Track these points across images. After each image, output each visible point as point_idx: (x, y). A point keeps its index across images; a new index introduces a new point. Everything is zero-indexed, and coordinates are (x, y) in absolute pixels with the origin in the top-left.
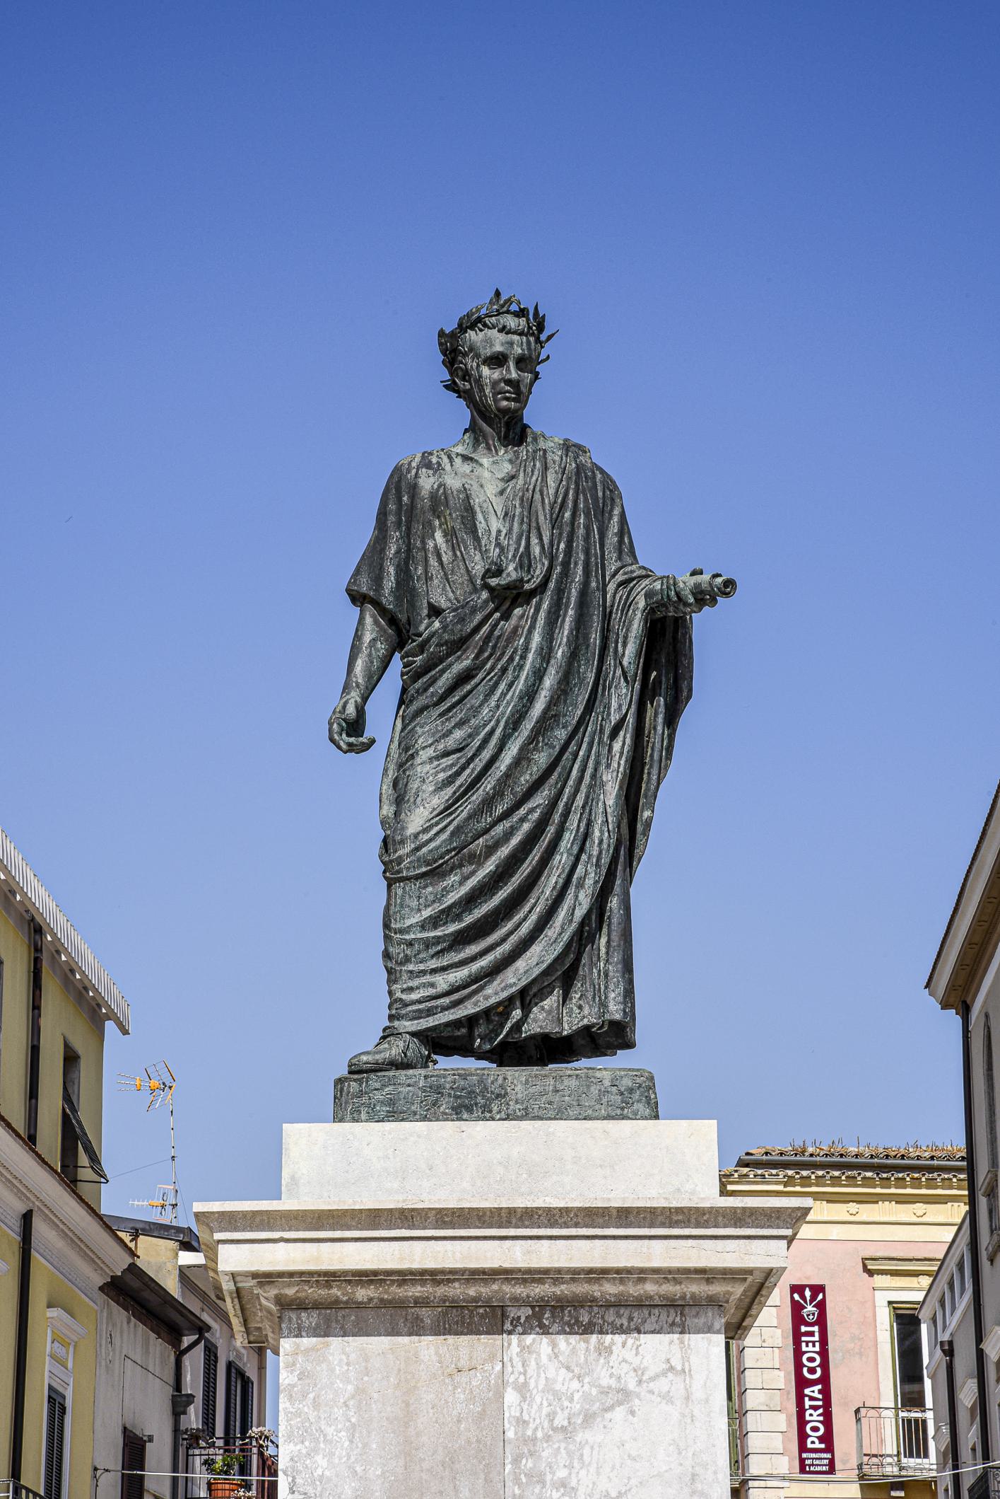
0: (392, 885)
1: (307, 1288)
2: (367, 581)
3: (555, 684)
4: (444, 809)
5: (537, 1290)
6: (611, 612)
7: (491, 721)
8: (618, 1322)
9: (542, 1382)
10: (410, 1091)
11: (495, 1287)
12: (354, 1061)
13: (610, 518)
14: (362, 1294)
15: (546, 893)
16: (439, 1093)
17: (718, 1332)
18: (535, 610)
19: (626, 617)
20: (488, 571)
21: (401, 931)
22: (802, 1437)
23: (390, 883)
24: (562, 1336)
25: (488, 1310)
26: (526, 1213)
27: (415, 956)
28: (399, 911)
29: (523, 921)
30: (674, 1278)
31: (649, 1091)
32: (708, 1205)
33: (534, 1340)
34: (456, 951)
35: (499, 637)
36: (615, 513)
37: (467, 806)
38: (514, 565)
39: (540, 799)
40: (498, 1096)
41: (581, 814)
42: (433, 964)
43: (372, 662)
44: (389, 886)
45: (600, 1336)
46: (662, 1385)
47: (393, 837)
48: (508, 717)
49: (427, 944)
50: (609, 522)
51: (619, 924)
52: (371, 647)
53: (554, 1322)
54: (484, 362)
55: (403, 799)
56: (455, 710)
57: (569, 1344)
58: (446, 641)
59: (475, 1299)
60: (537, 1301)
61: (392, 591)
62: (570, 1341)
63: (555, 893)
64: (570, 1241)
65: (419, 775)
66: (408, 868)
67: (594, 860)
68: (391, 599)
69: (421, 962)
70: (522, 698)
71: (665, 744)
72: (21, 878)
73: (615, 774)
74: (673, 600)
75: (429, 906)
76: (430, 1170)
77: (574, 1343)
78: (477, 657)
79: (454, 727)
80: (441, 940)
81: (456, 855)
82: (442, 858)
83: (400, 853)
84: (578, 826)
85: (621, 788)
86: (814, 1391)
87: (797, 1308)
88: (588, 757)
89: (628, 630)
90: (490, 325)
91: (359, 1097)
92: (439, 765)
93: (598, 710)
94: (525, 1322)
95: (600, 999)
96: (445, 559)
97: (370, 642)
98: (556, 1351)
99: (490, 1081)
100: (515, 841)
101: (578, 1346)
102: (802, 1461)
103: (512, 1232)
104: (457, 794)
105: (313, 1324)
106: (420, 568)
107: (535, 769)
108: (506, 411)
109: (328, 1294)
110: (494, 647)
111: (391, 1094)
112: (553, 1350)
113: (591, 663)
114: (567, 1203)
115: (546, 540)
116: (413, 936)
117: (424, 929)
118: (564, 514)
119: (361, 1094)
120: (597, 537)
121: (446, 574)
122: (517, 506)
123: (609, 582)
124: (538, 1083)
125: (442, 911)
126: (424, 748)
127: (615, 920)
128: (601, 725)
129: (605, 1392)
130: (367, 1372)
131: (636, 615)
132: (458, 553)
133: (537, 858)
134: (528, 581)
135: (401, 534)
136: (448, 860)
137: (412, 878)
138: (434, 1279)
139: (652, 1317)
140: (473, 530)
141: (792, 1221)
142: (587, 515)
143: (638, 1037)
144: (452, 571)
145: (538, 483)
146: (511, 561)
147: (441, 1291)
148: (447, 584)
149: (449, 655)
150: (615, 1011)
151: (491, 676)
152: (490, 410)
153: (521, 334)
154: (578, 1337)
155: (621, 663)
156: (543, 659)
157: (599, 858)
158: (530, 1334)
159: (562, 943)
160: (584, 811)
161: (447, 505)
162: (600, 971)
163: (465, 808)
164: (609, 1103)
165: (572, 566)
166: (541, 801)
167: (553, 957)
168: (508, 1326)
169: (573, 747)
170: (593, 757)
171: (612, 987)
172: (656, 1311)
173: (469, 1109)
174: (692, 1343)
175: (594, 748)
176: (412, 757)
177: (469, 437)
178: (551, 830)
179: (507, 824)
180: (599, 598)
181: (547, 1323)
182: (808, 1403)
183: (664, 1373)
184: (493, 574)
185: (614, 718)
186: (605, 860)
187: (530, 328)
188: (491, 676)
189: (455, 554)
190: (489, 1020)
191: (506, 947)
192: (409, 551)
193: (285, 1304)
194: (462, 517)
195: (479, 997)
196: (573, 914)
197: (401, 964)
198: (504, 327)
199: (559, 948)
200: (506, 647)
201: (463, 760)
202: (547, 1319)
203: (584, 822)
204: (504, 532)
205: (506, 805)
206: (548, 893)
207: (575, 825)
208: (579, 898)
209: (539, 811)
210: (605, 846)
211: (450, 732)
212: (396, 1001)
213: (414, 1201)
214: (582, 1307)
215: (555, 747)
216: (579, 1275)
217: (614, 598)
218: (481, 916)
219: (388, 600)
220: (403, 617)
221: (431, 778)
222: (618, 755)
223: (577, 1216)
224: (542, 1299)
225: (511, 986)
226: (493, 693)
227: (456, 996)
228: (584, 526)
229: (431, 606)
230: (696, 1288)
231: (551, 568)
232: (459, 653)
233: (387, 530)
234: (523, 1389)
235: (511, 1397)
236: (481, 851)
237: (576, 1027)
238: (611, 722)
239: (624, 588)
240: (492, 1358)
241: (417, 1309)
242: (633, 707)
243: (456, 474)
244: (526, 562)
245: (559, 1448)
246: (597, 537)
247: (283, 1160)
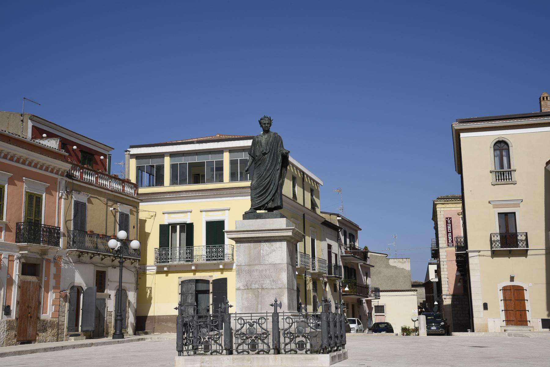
5: (264, 239)
22: (448, 241)
39: (269, 179)
42: (256, 200)
46: (279, 249)
49: (255, 197)
86: (450, 234)
87: (447, 221)
100: (266, 184)
102: (448, 245)
129: (272, 250)
130: (245, 249)
147: (253, 239)
150: (279, 204)
153: (267, 120)
169: (273, 172)
173: (258, 218)
182: (449, 236)
183: (279, 248)
185: (278, 168)
191: (264, 198)
195: (261, 204)
231: (270, 150)
234: (263, 250)
235: (262, 251)
240: (259, 247)
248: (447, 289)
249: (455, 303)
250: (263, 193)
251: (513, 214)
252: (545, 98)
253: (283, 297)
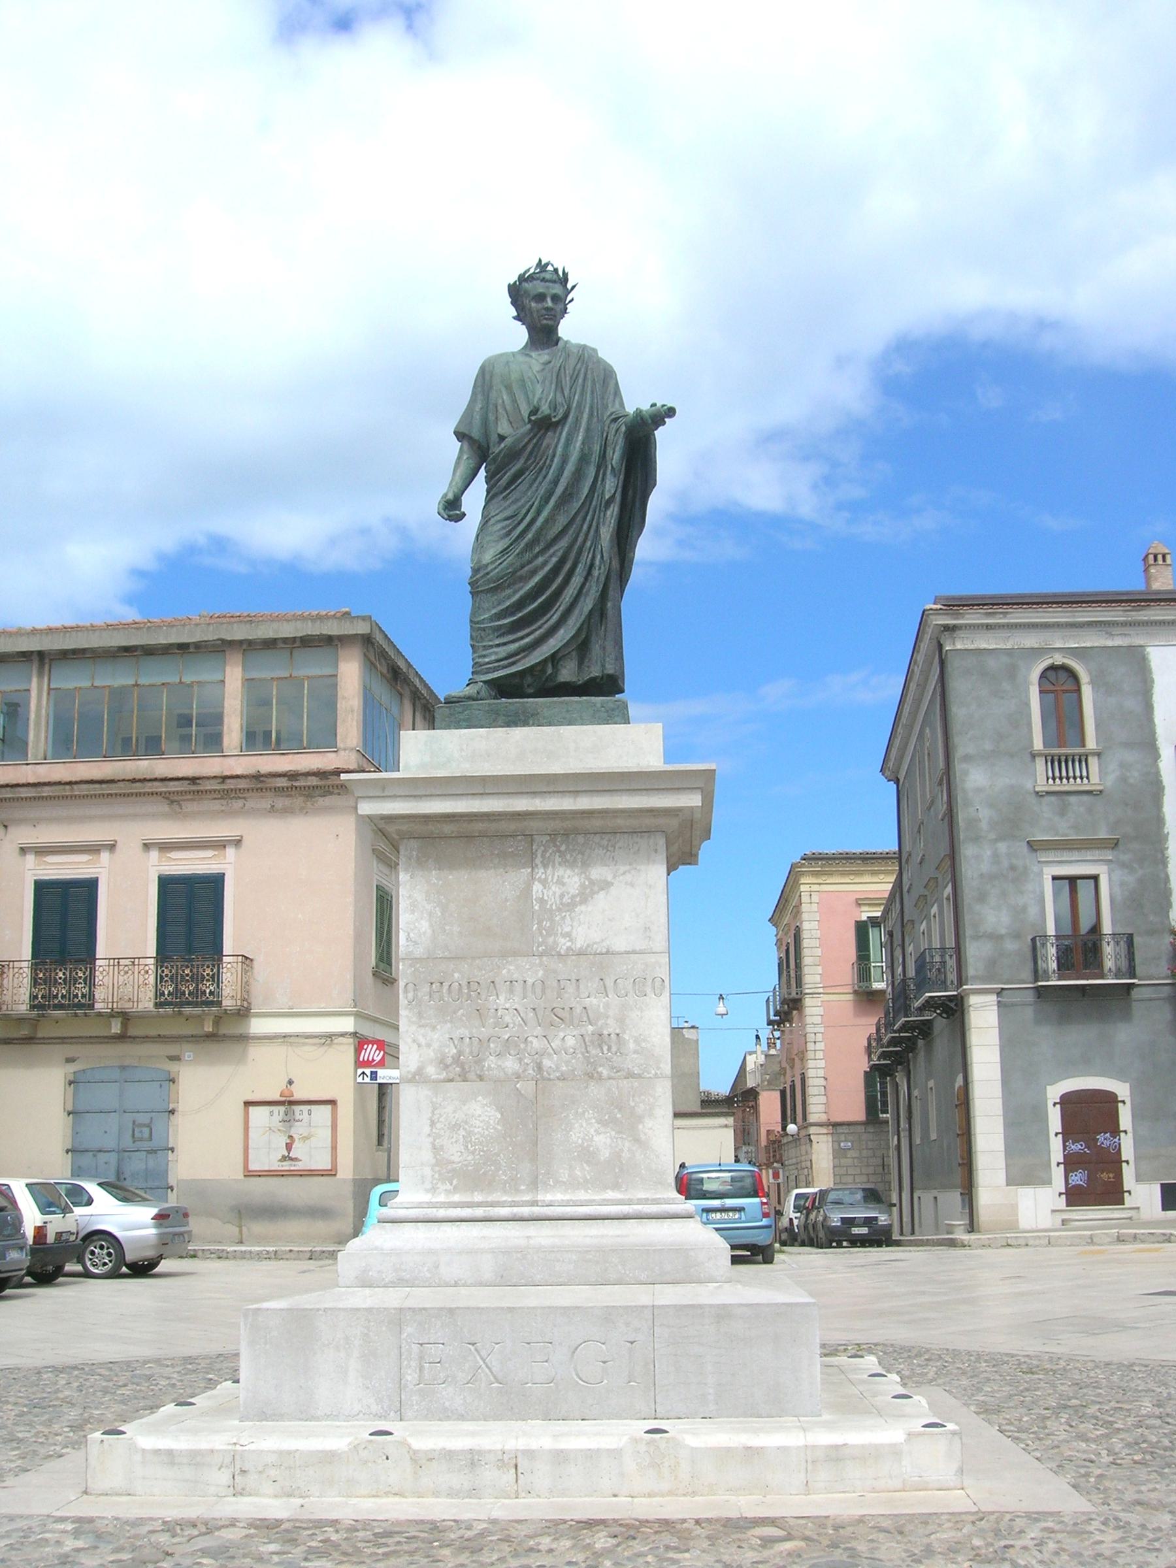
5: (551, 825)
9: (556, 877)
11: (525, 823)
39: (563, 543)
42: (497, 642)
78: (525, 463)
88: (593, 520)
110: (536, 458)
134: (555, 417)
136: (507, 580)
143: (626, 688)
150: (610, 669)
169: (582, 514)
181: (558, 844)
190: (532, 675)
191: (542, 631)
201: (516, 522)
209: (562, 551)
227: (510, 660)
242: (620, 490)
245: (565, 916)
247: (438, 776)
248: (821, 1108)
249: (842, 1144)
250: (535, 611)
251: (1092, 881)
252: (1160, 557)
253: (649, 1123)
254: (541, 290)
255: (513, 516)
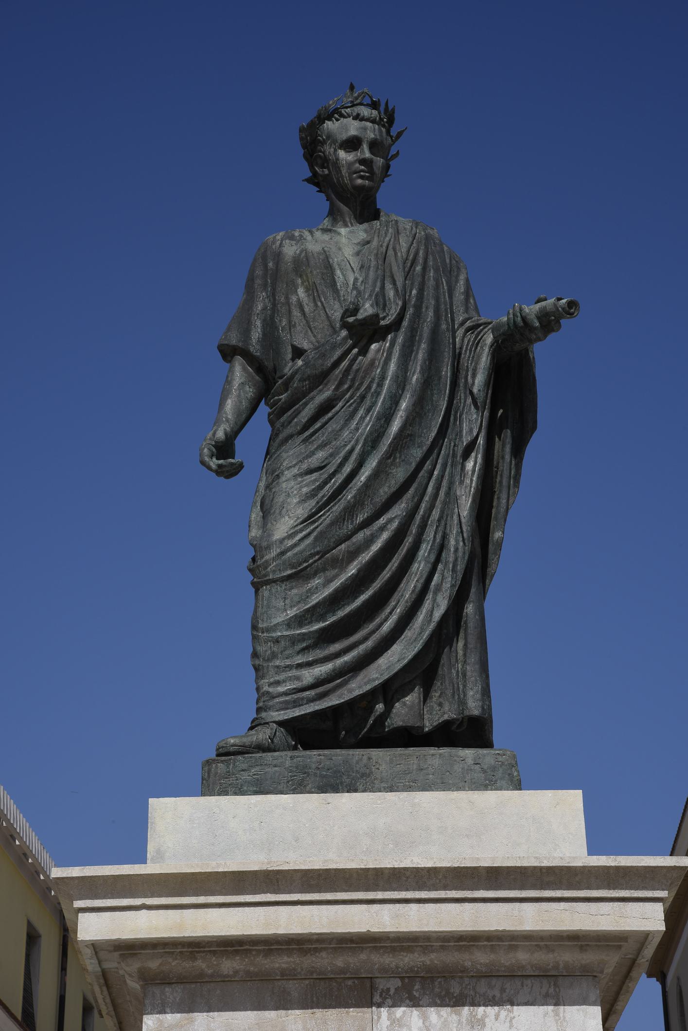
0: (259, 590)
1: (170, 960)
2: (236, 335)
3: (411, 405)
4: (307, 517)
5: (407, 960)
6: (460, 354)
7: (350, 442)
8: (490, 993)
10: (276, 771)
11: (363, 956)
12: (222, 744)
13: (457, 281)
14: (228, 965)
15: (406, 596)
16: (305, 773)
17: (594, 1004)
18: (390, 344)
19: (474, 353)
20: (346, 311)
21: (268, 630)
23: (257, 587)
24: (432, 1009)
25: (356, 982)
26: (439, 590)
27: (282, 652)
28: (266, 612)
29: (385, 622)
30: (546, 945)
31: (512, 769)
32: (580, 864)
33: (404, 1012)
34: (320, 648)
35: (358, 371)
36: (460, 278)
37: (329, 515)
38: (371, 302)
39: (399, 510)
40: (363, 775)
41: (437, 527)
42: (300, 659)
43: (241, 402)
44: (257, 591)
45: (472, 1008)
47: (260, 544)
48: (367, 436)
50: (456, 285)
51: (475, 628)
52: (240, 390)
53: (424, 994)
54: (341, 147)
55: (269, 512)
56: (317, 434)
57: (440, 1016)
58: (309, 376)
59: (342, 971)
60: (406, 972)
61: (258, 341)
62: (442, 1013)
63: (414, 596)
64: (438, 905)
65: (284, 491)
66: (274, 572)
67: (451, 566)
68: (258, 347)
69: (287, 658)
70: (380, 419)
71: (513, 473)
72: (5, 798)
73: (467, 491)
74: (520, 325)
75: (294, 606)
76: (295, 841)
77: (445, 1015)
79: (316, 449)
80: (306, 637)
81: (319, 559)
82: (306, 561)
83: (267, 557)
84: (435, 537)
85: (474, 500)
88: (443, 476)
89: (477, 364)
90: (345, 114)
91: (227, 778)
92: (303, 481)
93: (451, 437)
94: (394, 994)
95: (459, 697)
96: (307, 309)
97: (239, 385)
98: (427, 1024)
99: (354, 761)
100: (376, 547)
101: (450, 1019)
103: (380, 895)
104: (320, 503)
105: (178, 999)
106: (284, 320)
107: (393, 482)
108: (361, 188)
109: (193, 967)
110: (353, 380)
111: (257, 774)
112: (423, 1023)
113: (443, 392)
114: (435, 863)
115: (399, 284)
116: (279, 634)
117: (289, 627)
118: (415, 268)
119: (228, 774)
120: (446, 288)
121: (308, 322)
122: (372, 260)
123: (458, 329)
124: (402, 762)
125: (308, 610)
126: (288, 468)
127: (471, 625)
128: (454, 450)
131: (483, 350)
132: (319, 304)
133: (396, 565)
134: (384, 318)
135: (267, 294)
136: (312, 564)
137: (277, 580)
138: (300, 948)
139: (525, 987)
140: (333, 284)
141: (667, 882)
142: (437, 270)
144: (314, 318)
145: (391, 243)
146: (367, 299)
147: (308, 962)
148: (309, 331)
149: (311, 390)
150: (474, 708)
151: (350, 403)
152: (346, 189)
154: (449, 1009)
155: (471, 393)
156: (398, 386)
157: (454, 566)
158: (400, 1006)
159: (421, 641)
160: (439, 524)
161: (308, 265)
162: (458, 671)
163: (327, 517)
164: (473, 781)
165: (424, 310)
166: (399, 513)
167: (413, 653)
168: (377, 998)
169: (428, 465)
170: (446, 477)
171: (470, 685)
172: (528, 982)
174: (568, 1016)
175: (448, 470)
176: (278, 476)
177: (328, 221)
178: (409, 540)
179: (367, 532)
180: (449, 337)
184: (351, 313)
185: (466, 440)
186: (461, 567)
187: (380, 118)
188: (350, 403)
189: (316, 305)
191: (370, 644)
192: (274, 305)
193: (149, 979)
194: (323, 274)
196: (431, 616)
197: (269, 660)
198: (358, 115)
199: (419, 646)
200: (364, 378)
201: (326, 476)
202: (417, 991)
203: (440, 535)
204: (361, 279)
205: (366, 514)
206: (407, 596)
207: (432, 536)
208: (437, 601)
210: (460, 554)
211: (313, 453)
212: (263, 694)
213: (279, 863)
214: (453, 977)
215: (411, 463)
216: (449, 942)
217: (463, 341)
218: (344, 616)
219: (255, 348)
220: (269, 364)
221: (295, 492)
222: (470, 473)
223: (446, 877)
224: (411, 970)
225: (374, 680)
226: (352, 418)
228: (434, 279)
229: (294, 347)
230: (568, 957)
231: (404, 309)
232: (321, 387)
233: (254, 292)
236: (343, 556)
237: (437, 723)
238: (463, 443)
239: (472, 333)
241: (284, 982)
243: (316, 241)
244: (381, 301)
246: (446, 288)
254: (353, 132)
255: (320, 468)
